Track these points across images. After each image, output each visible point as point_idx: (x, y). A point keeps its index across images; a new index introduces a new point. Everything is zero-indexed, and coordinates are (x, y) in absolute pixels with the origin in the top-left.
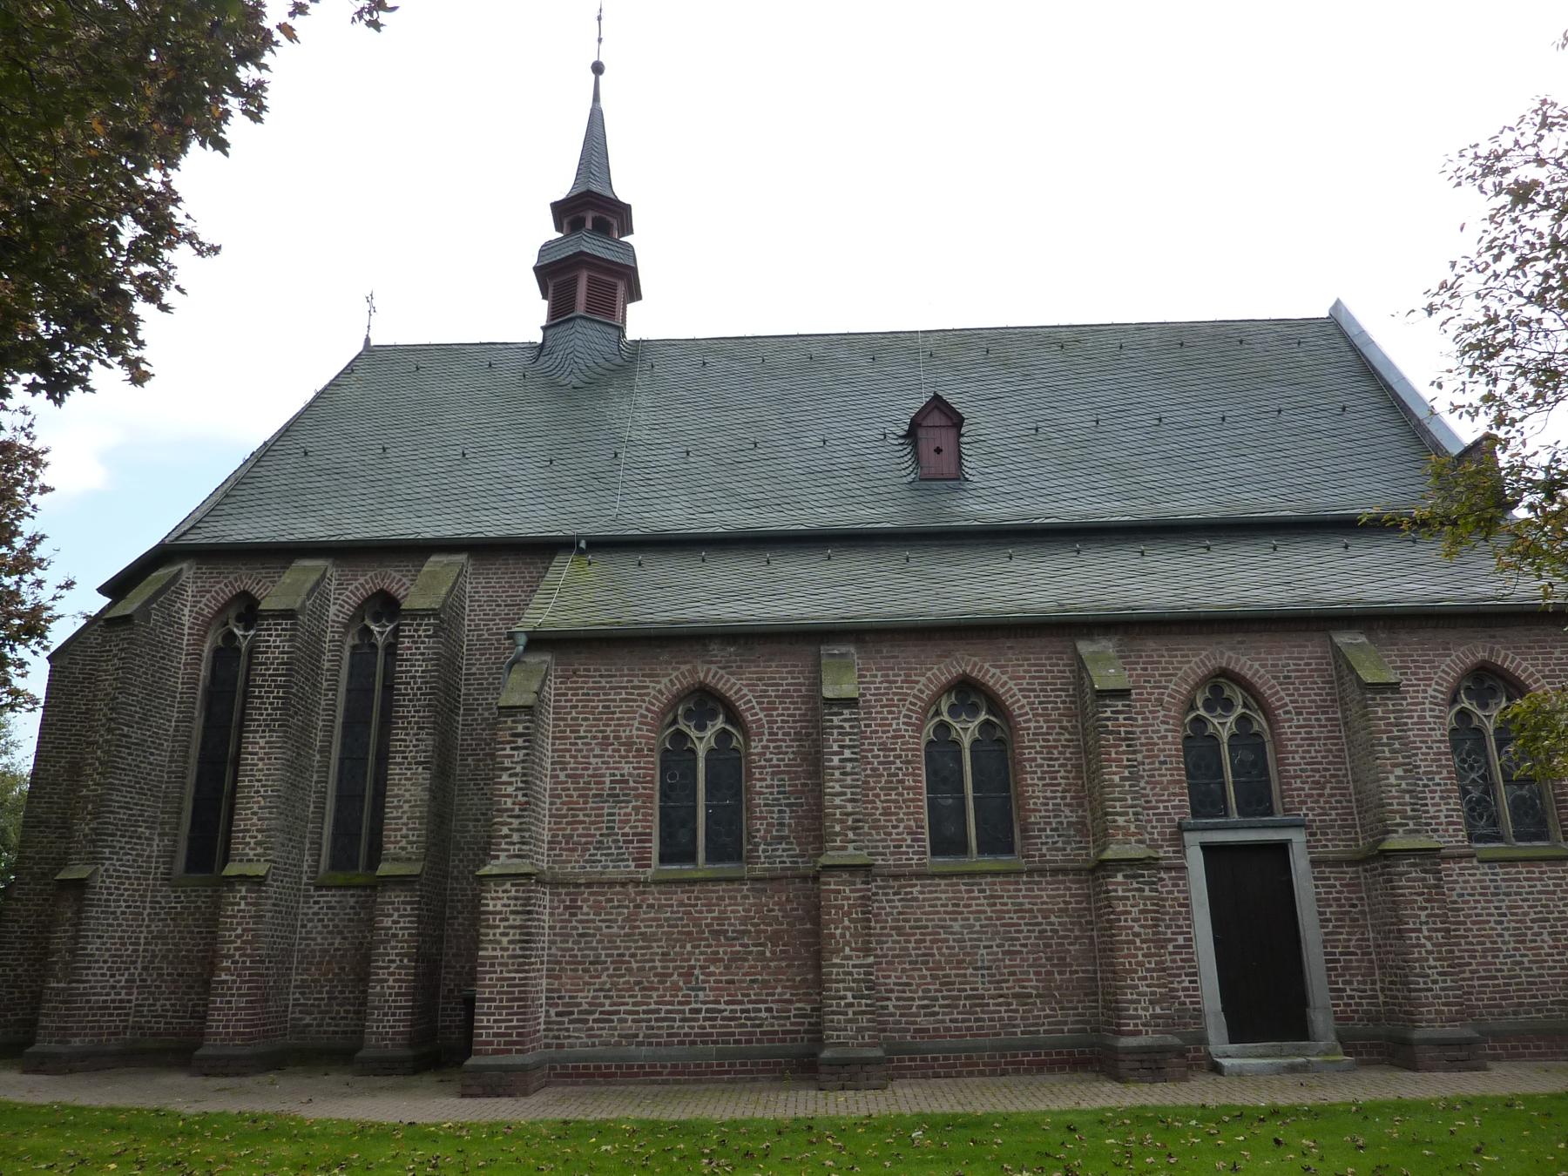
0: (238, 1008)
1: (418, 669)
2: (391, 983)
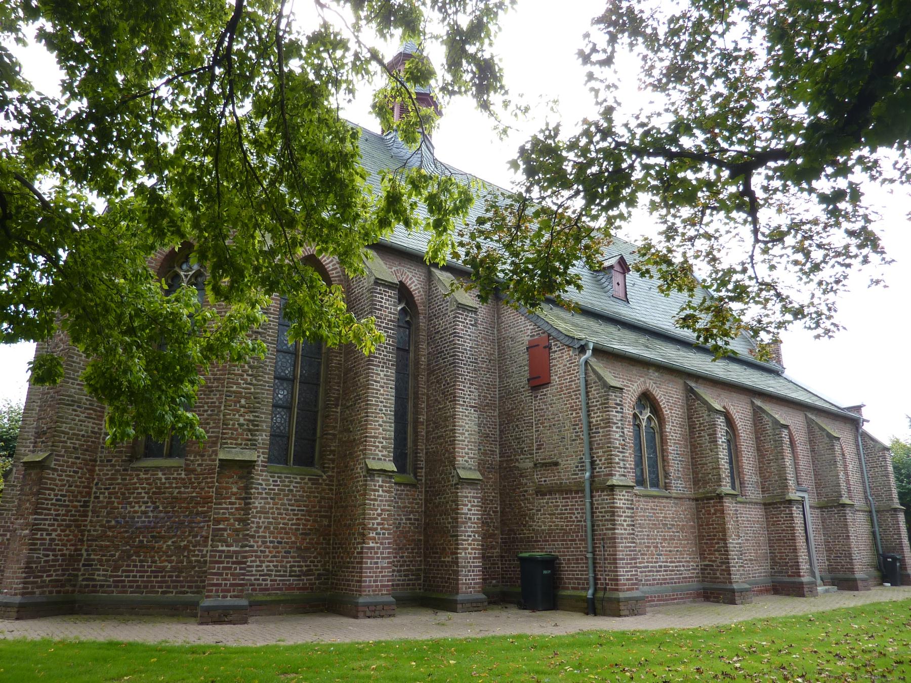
0: (382, 568)
1: (468, 345)
2: (470, 551)
